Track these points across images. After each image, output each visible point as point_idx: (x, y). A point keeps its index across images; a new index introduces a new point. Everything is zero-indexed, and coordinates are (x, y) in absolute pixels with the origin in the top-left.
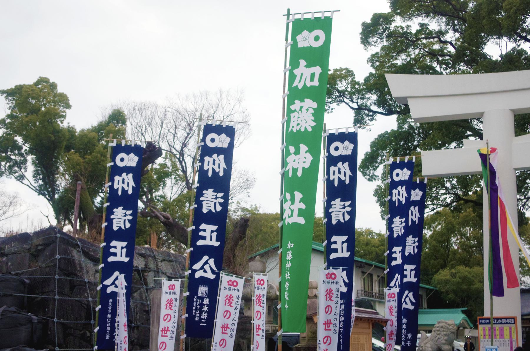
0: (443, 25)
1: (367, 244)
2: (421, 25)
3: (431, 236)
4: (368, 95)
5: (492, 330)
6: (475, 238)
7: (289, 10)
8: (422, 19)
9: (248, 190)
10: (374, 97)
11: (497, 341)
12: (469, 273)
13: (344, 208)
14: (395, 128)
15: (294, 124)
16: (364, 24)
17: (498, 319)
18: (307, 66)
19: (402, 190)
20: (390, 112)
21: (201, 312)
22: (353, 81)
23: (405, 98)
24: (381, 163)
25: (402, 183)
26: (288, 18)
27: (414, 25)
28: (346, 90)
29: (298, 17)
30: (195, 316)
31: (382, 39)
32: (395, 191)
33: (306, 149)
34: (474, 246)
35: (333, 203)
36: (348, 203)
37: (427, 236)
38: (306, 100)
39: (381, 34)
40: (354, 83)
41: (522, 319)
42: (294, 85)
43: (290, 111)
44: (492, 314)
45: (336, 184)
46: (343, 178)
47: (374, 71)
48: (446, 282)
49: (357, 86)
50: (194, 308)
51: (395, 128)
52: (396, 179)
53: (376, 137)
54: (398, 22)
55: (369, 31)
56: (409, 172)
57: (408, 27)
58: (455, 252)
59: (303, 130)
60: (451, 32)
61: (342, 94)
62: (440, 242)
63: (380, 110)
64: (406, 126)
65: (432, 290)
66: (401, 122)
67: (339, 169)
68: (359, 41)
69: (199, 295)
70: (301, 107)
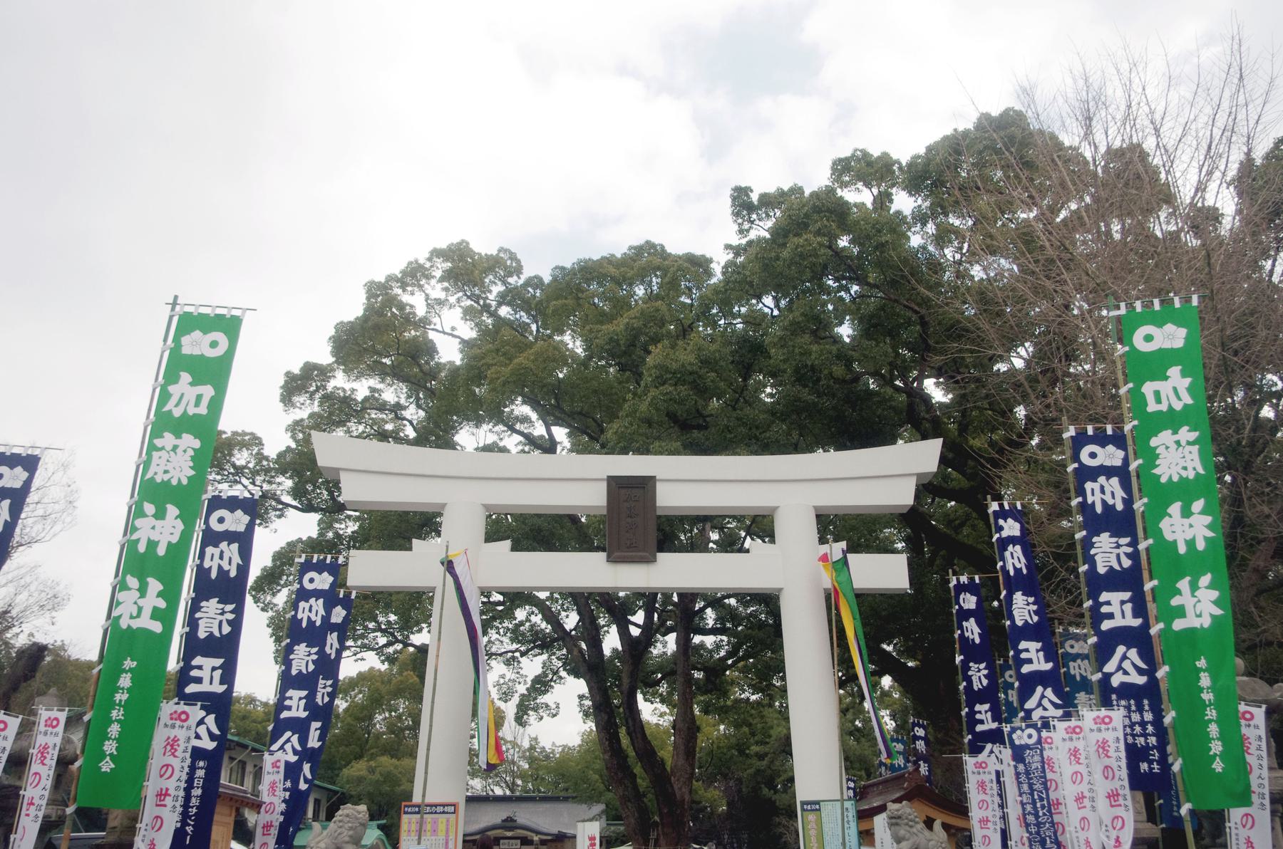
0: (403, 397)
1: (244, 718)
2: (373, 390)
3: (346, 710)
4: (280, 479)
5: (421, 824)
6: (410, 715)
7: (176, 297)
8: (374, 382)
9: (54, 614)
10: (289, 483)
11: (427, 839)
12: (396, 767)
13: (222, 614)
14: (315, 535)
15: (160, 470)
16: (288, 374)
17: (431, 806)
18: (192, 384)
19: (318, 605)
20: (309, 508)
22: (259, 453)
23: (337, 470)
24: (285, 585)
25: (317, 594)
26: (173, 309)
27: (361, 388)
28: (245, 467)
29: (188, 309)
31: (311, 398)
33: (177, 512)
34: (408, 728)
35: (203, 604)
36: (230, 607)
37: (341, 710)
38: (184, 435)
39: (312, 394)
40: (260, 457)
41: (464, 841)
42: (166, 408)
43: (152, 448)
44: (424, 796)
45: (214, 575)
46: (226, 567)
47: (293, 445)
48: (360, 780)
49: (265, 463)
51: (315, 535)
53: (283, 544)
54: (340, 381)
55: (295, 386)
56: (331, 579)
57: (353, 390)
58: (379, 736)
59: (174, 482)
60: (413, 408)
61: (239, 470)
62: (359, 719)
63: (295, 503)
64: (330, 535)
65: (336, 792)
66: (325, 526)
67: (222, 552)
68: (278, 397)
70: (175, 448)
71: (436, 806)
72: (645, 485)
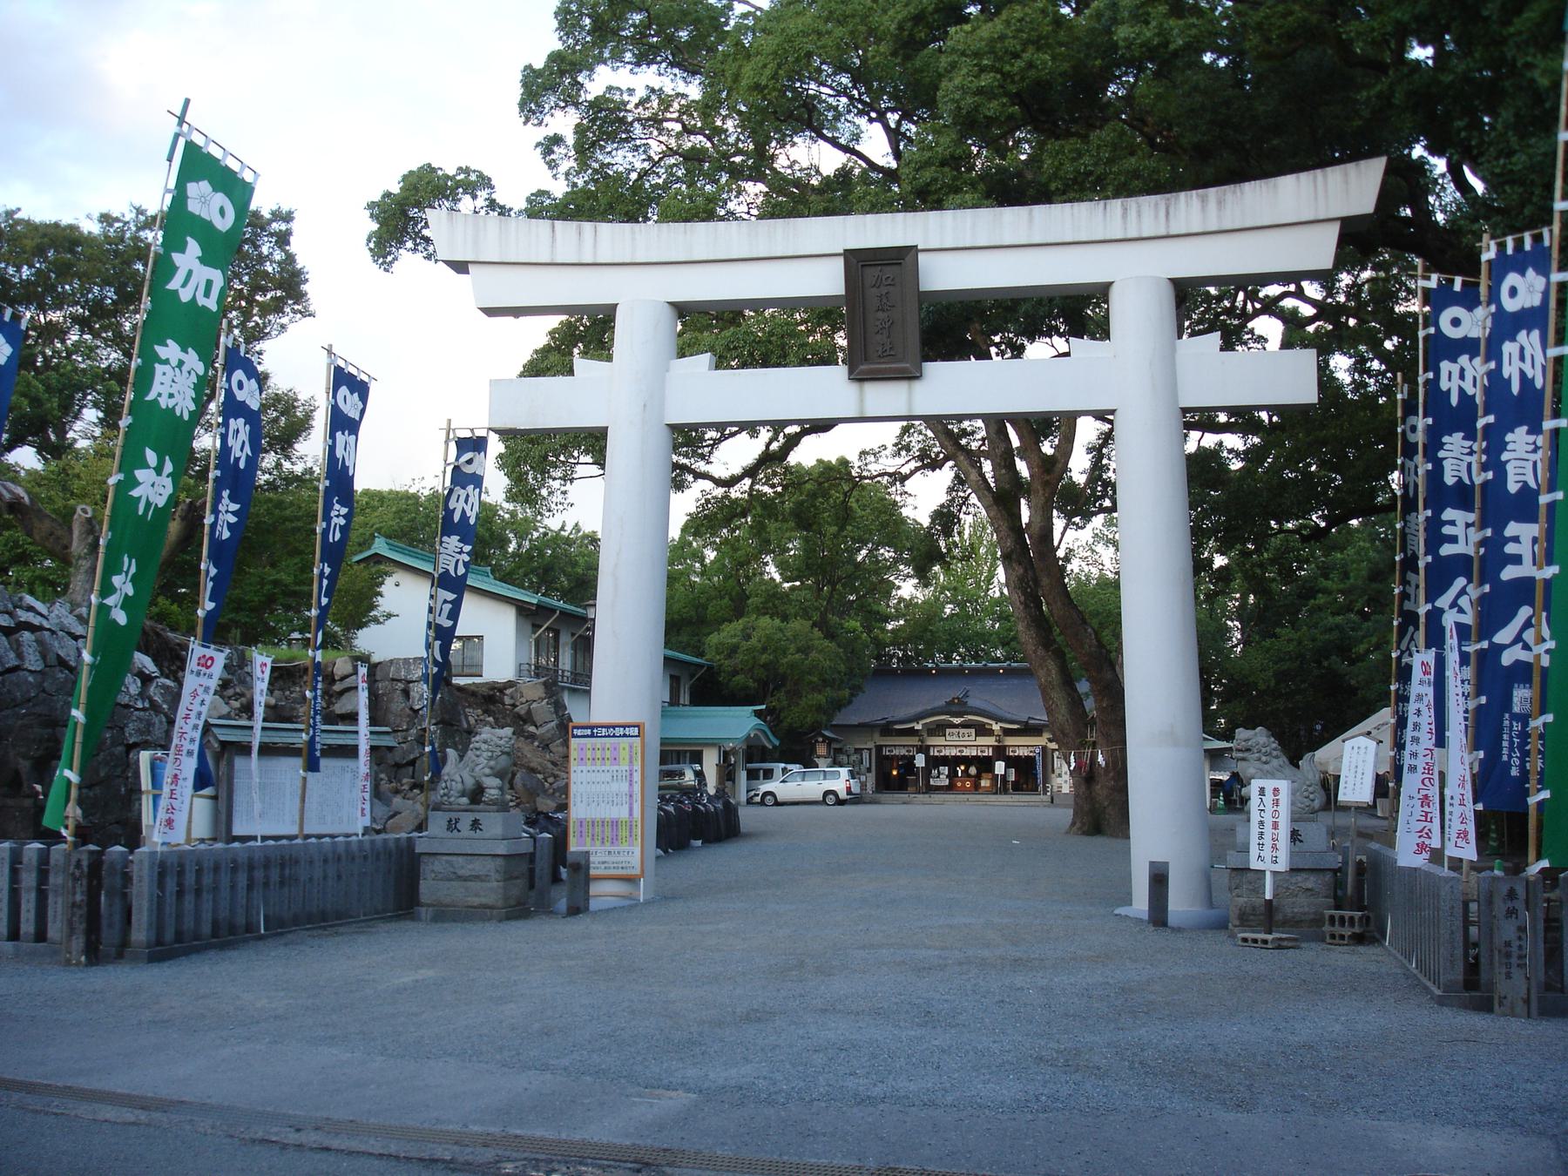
21: (1525, 754)
30: (1508, 765)
32: (1508, 348)
50: (1505, 744)
52: (1510, 305)
69: (1516, 709)
71: (614, 727)
72: (902, 258)
